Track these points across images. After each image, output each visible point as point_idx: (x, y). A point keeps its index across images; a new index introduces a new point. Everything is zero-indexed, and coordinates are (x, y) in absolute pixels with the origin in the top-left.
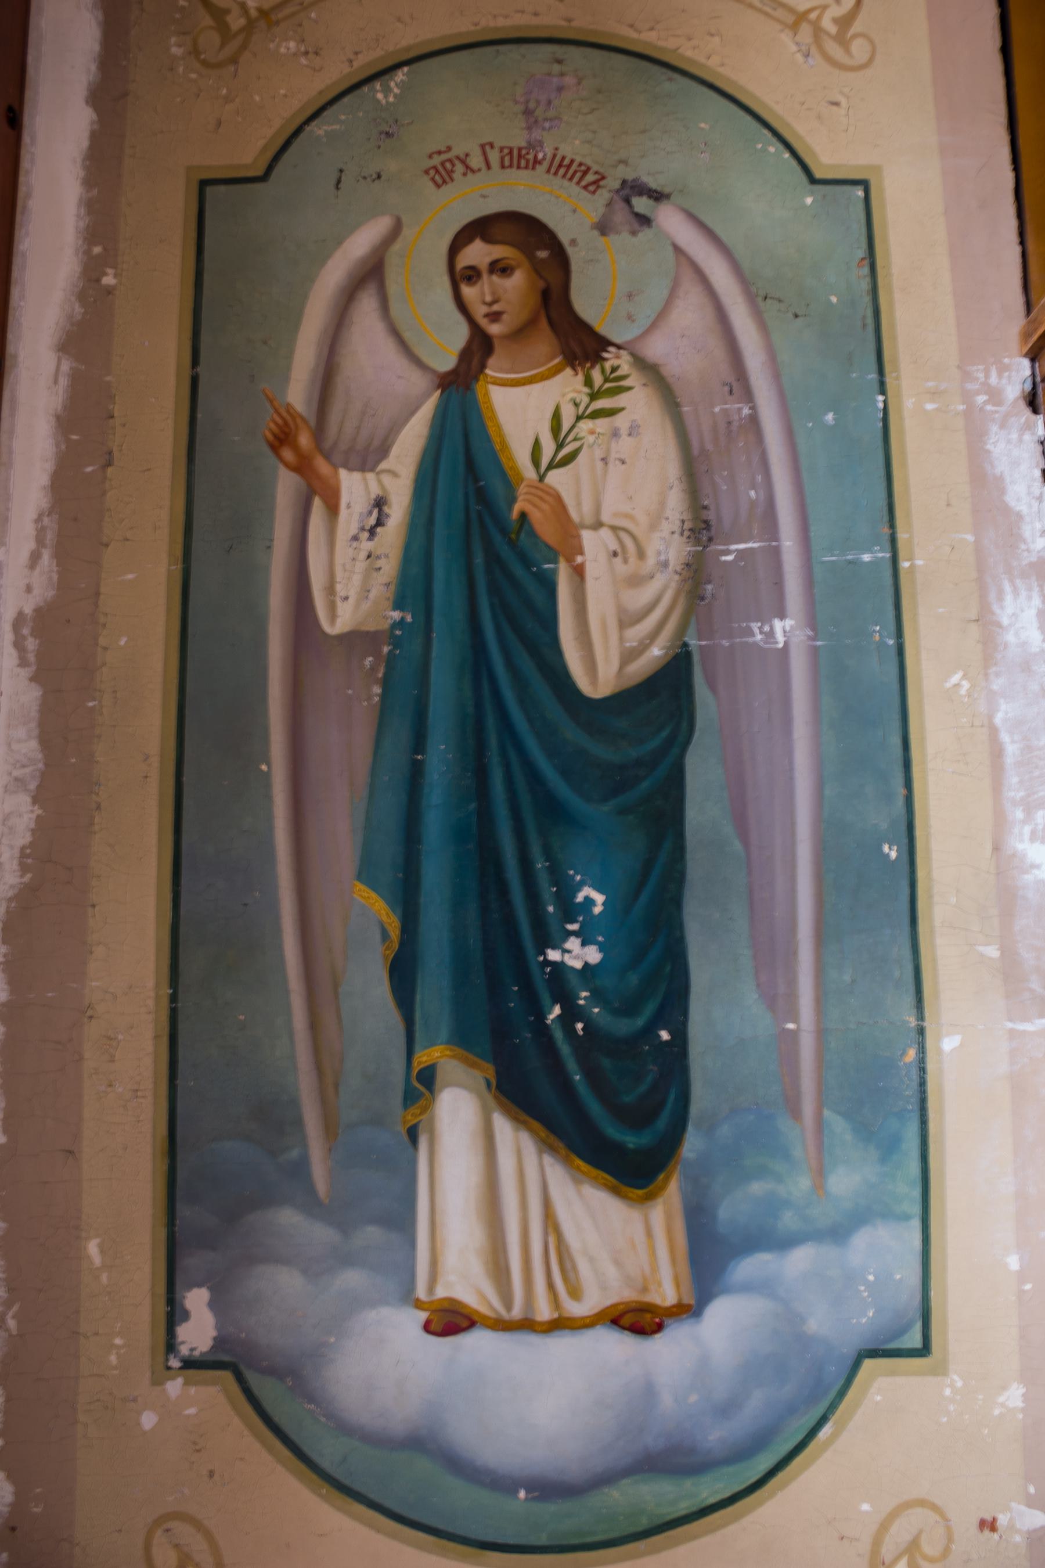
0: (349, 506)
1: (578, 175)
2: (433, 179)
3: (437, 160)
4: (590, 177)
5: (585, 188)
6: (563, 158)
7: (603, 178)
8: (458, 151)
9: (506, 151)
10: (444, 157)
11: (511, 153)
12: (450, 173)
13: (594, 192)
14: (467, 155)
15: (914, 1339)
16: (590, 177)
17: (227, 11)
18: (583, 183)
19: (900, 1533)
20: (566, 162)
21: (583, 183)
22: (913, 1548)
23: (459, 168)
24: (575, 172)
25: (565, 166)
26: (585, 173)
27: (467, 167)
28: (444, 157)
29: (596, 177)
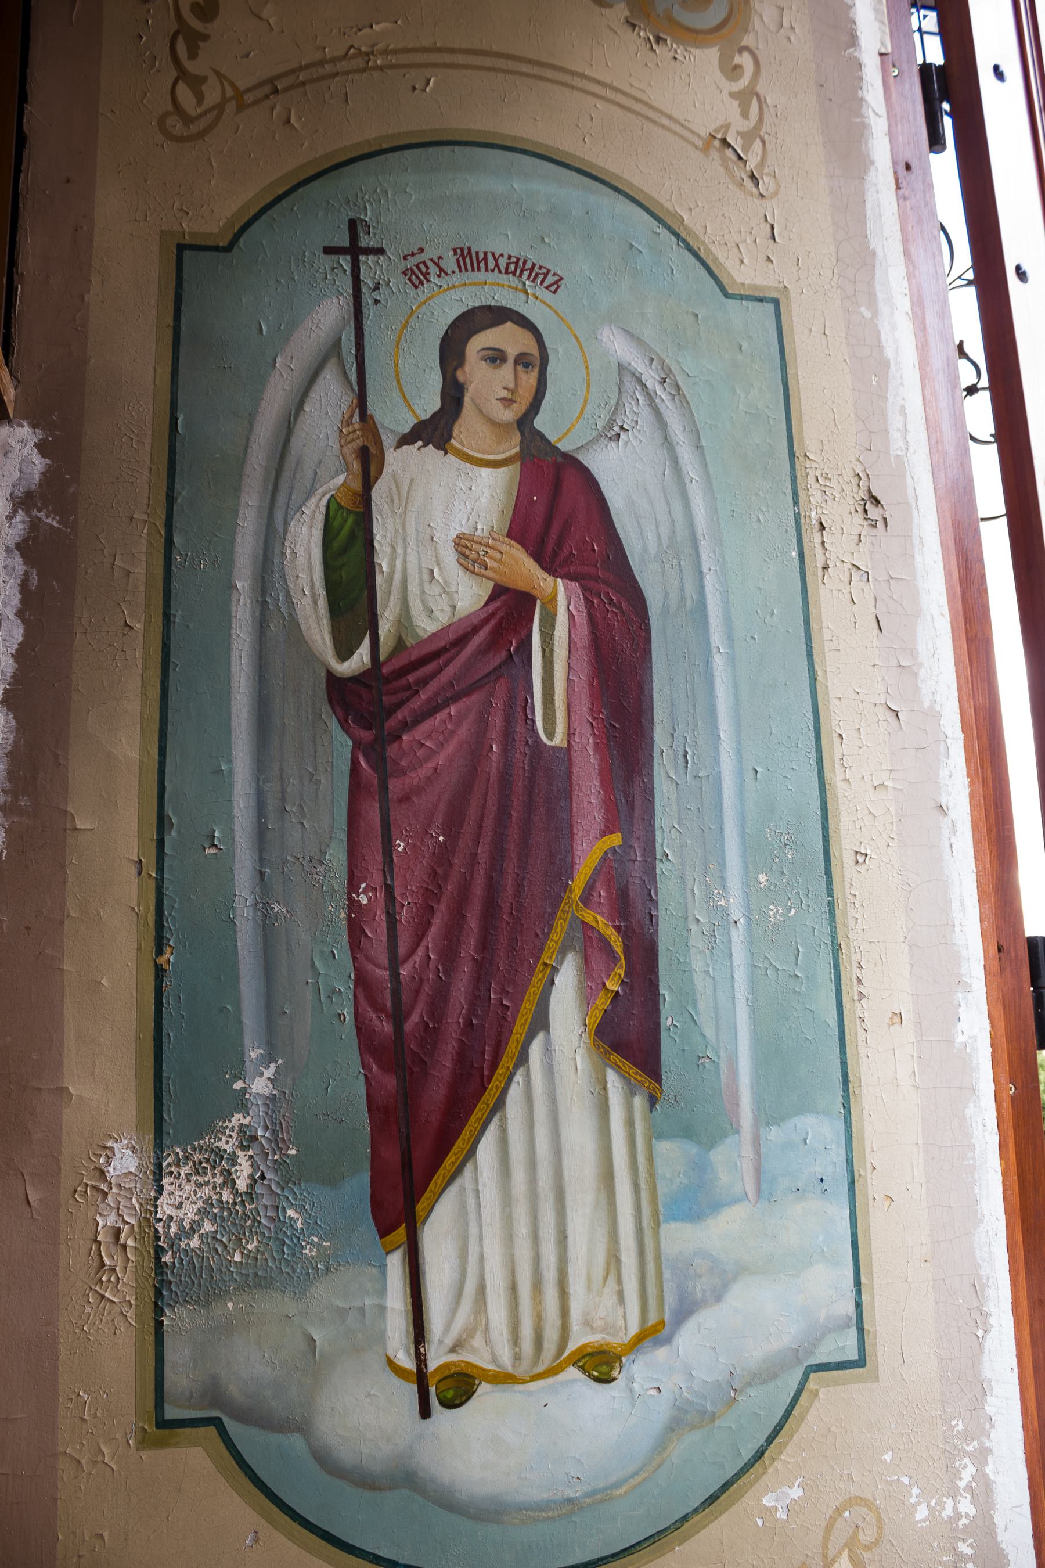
0: (499, 1295)
1: (541, 277)
2: (410, 279)
3: (411, 262)
4: (550, 279)
5: (547, 288)
6: (477, 253)
7: (561, 279)
8: (430, 253)
9: (514, 260)
10: (418, 259)
11: (517, 263)
12: (426, 275)
13: (555, 292)
14: (440, 258)
15: (847, 1346)
16: (550, 279)
17: (204, 79)
18: (545, 285)
19: (840, 1535)
20: (529, 265)
21: (545, 285)
22: (851, 1544)
23: (434, 270)
24: (537, 275)
25: (527, 270)
26: (546, 275)
27: (441, 270)
28: (418, 259)
29: (556, 278)
